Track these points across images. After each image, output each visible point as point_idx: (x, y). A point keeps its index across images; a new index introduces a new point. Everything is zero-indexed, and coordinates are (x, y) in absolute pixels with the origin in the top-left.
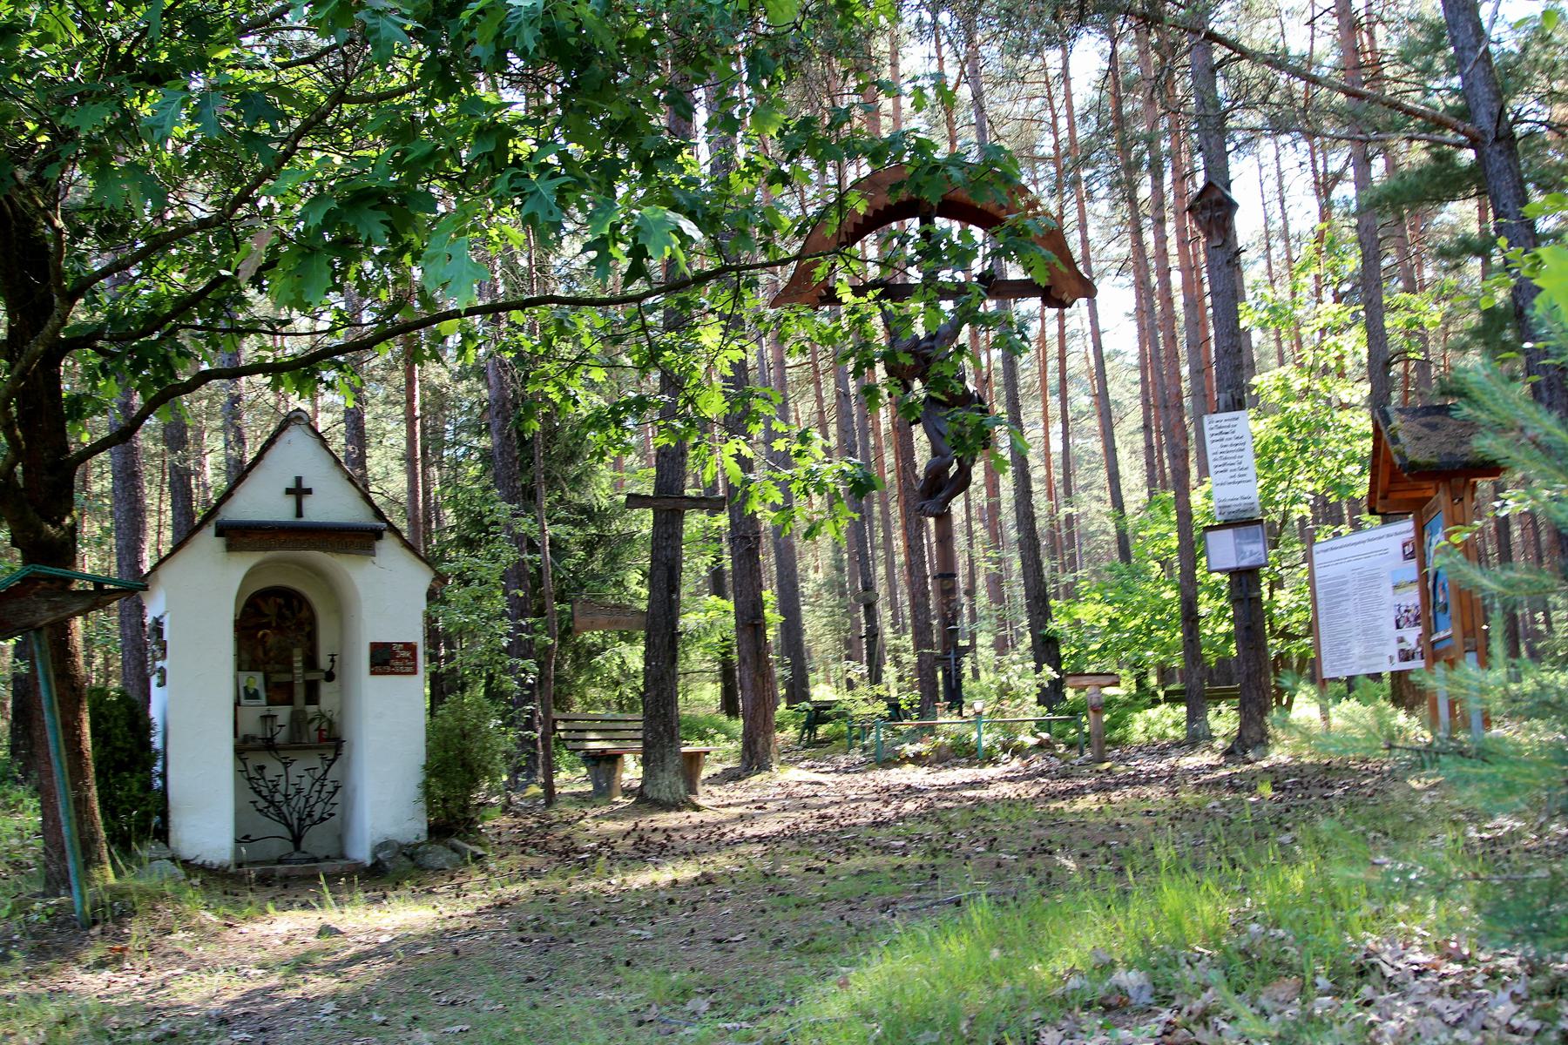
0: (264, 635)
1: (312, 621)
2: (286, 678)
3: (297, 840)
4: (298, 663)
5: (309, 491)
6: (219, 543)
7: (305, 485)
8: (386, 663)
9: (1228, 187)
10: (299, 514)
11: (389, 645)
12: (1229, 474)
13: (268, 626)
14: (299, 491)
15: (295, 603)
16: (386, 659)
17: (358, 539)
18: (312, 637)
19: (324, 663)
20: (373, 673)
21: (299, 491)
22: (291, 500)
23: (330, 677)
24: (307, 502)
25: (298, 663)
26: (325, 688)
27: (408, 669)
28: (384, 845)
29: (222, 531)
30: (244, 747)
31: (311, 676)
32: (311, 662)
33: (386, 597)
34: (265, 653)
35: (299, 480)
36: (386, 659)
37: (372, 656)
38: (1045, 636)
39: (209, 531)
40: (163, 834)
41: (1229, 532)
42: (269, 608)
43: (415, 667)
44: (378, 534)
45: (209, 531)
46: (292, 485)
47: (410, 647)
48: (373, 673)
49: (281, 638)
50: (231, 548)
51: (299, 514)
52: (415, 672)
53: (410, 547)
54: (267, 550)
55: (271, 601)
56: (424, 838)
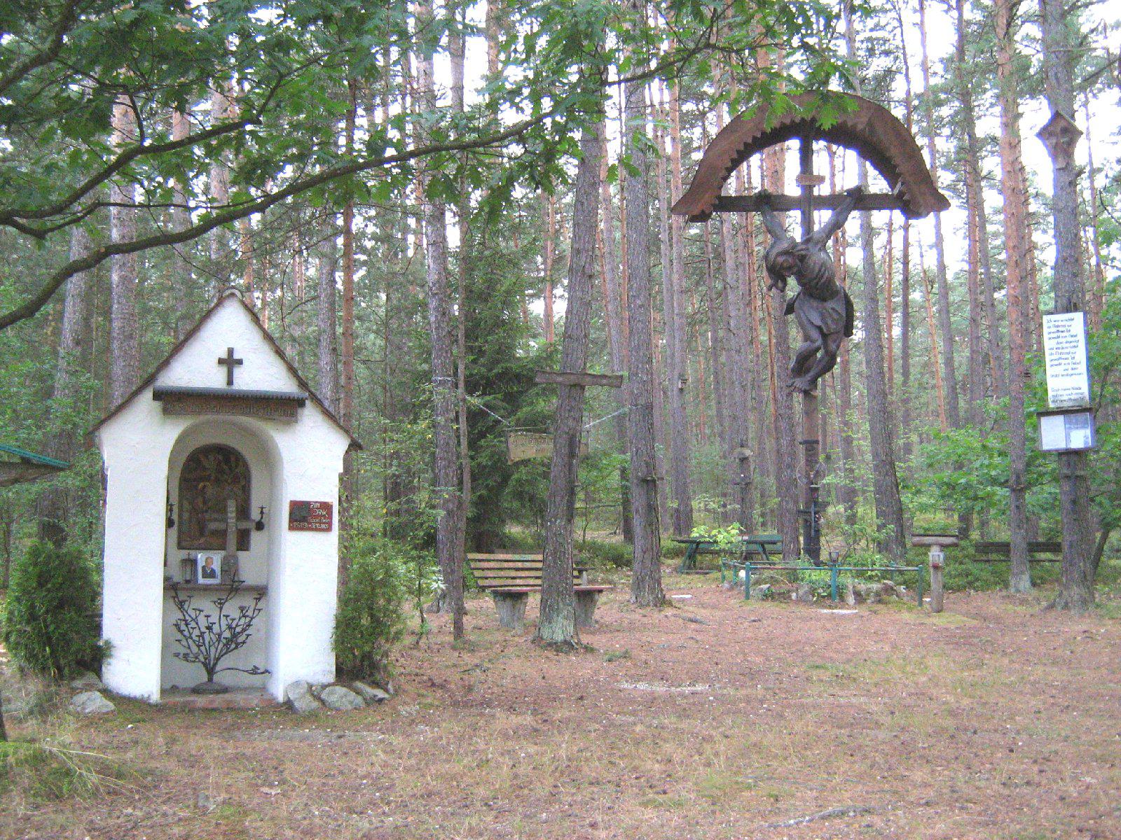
0: (204, 487)
1: (247, 477)
2: (222, 526)
3: (211, 671)
4: (232, 514)
5: (240, 362)
6: (157, 405)
7: (236, 356)
8: (304, 519)
9: (1073, 117)
10: (230, 382)
11: (309, 503)
12: (1063, 367)
13: (208, 479)
14: (230, 362)
15: (233, 459)
16: (306, 516)
17: (281, 408)
18: (246, 490)
19: (255, 515)
20: (291, 528)
21: (230, 362)
22: (223, 371)
23: (260, 526)
24: (237, 372)
25: (232, 514)
26: (255, 537)
27: (323, 526)
28: (297, 684)
29: (158, 396)
30: (172, 589)
31: (244, 525)
32: (244, 512)
33: (310, 459)
34: (205, 502)
35: (231, 352)
36: (306, 516)
37: (291, 514)
38: (224, 549)
39: (148, 395)
40: (98, 672)
41: (1060, 418)
42: (210, 463)
43: (330, 524)
44: (300, 403)
45: (148, 395)
46: (224, 356)
47: (327, 507)
48: (291, 528)
49: (216, 494)
50: (166, 411)
51: (230, 382)
52: (329, 529)
53: (327, 413)
54: (199, 413)
55: (211, 457)
56: (331, 678)
